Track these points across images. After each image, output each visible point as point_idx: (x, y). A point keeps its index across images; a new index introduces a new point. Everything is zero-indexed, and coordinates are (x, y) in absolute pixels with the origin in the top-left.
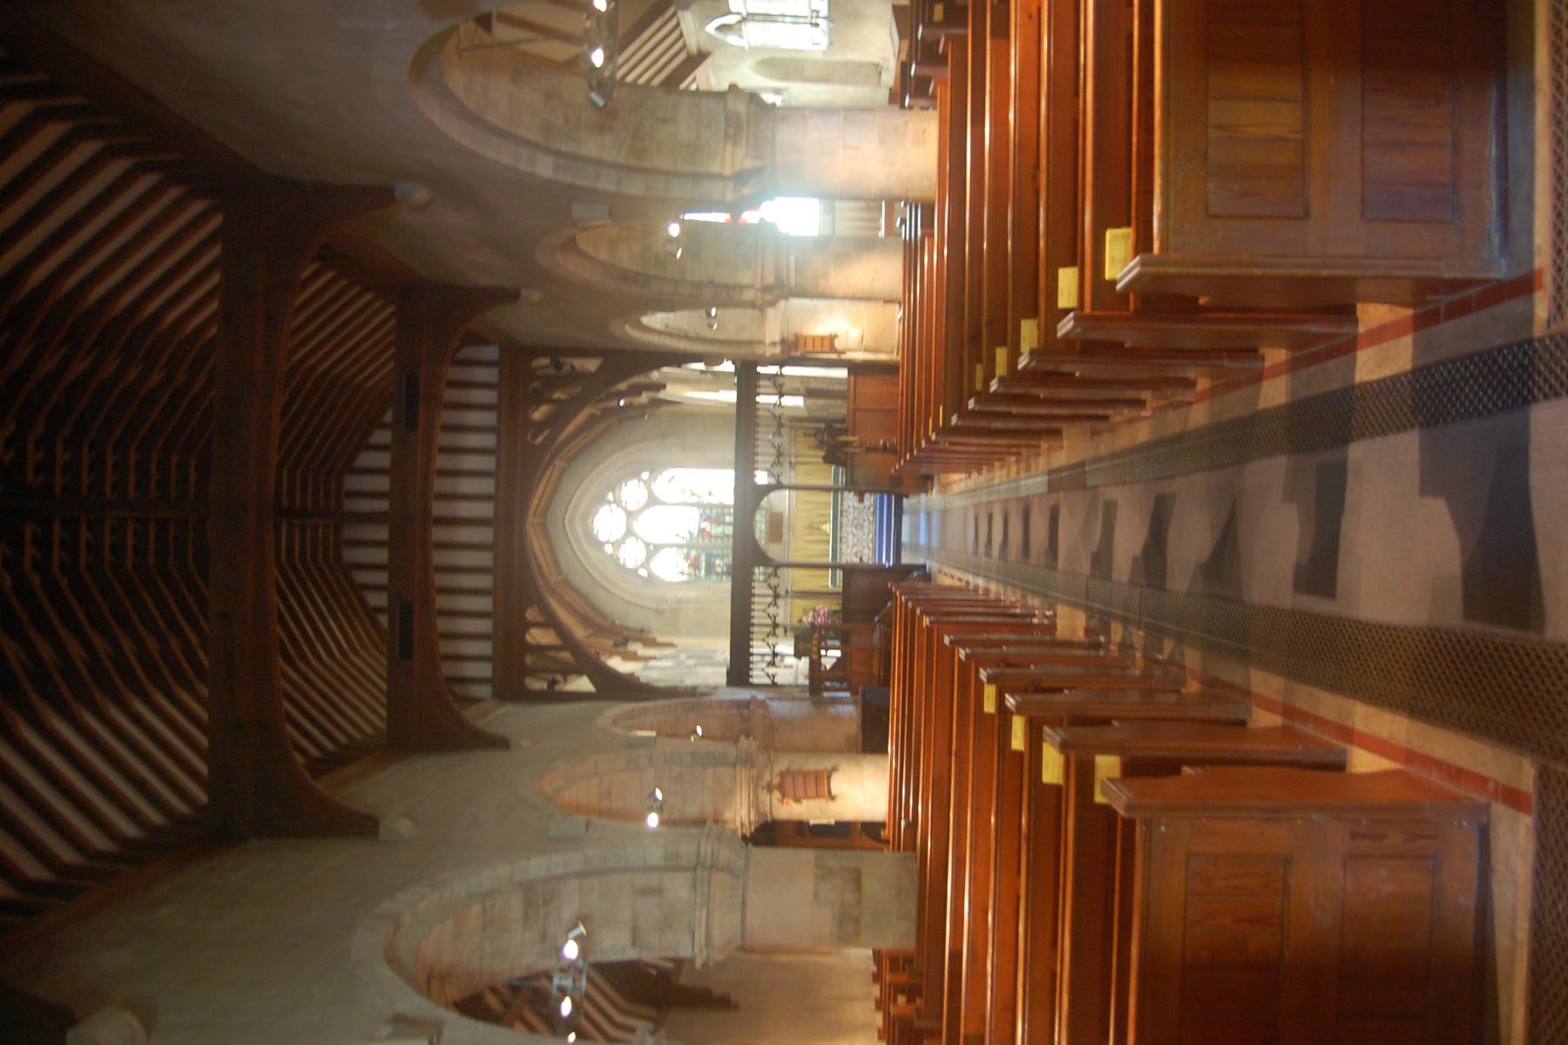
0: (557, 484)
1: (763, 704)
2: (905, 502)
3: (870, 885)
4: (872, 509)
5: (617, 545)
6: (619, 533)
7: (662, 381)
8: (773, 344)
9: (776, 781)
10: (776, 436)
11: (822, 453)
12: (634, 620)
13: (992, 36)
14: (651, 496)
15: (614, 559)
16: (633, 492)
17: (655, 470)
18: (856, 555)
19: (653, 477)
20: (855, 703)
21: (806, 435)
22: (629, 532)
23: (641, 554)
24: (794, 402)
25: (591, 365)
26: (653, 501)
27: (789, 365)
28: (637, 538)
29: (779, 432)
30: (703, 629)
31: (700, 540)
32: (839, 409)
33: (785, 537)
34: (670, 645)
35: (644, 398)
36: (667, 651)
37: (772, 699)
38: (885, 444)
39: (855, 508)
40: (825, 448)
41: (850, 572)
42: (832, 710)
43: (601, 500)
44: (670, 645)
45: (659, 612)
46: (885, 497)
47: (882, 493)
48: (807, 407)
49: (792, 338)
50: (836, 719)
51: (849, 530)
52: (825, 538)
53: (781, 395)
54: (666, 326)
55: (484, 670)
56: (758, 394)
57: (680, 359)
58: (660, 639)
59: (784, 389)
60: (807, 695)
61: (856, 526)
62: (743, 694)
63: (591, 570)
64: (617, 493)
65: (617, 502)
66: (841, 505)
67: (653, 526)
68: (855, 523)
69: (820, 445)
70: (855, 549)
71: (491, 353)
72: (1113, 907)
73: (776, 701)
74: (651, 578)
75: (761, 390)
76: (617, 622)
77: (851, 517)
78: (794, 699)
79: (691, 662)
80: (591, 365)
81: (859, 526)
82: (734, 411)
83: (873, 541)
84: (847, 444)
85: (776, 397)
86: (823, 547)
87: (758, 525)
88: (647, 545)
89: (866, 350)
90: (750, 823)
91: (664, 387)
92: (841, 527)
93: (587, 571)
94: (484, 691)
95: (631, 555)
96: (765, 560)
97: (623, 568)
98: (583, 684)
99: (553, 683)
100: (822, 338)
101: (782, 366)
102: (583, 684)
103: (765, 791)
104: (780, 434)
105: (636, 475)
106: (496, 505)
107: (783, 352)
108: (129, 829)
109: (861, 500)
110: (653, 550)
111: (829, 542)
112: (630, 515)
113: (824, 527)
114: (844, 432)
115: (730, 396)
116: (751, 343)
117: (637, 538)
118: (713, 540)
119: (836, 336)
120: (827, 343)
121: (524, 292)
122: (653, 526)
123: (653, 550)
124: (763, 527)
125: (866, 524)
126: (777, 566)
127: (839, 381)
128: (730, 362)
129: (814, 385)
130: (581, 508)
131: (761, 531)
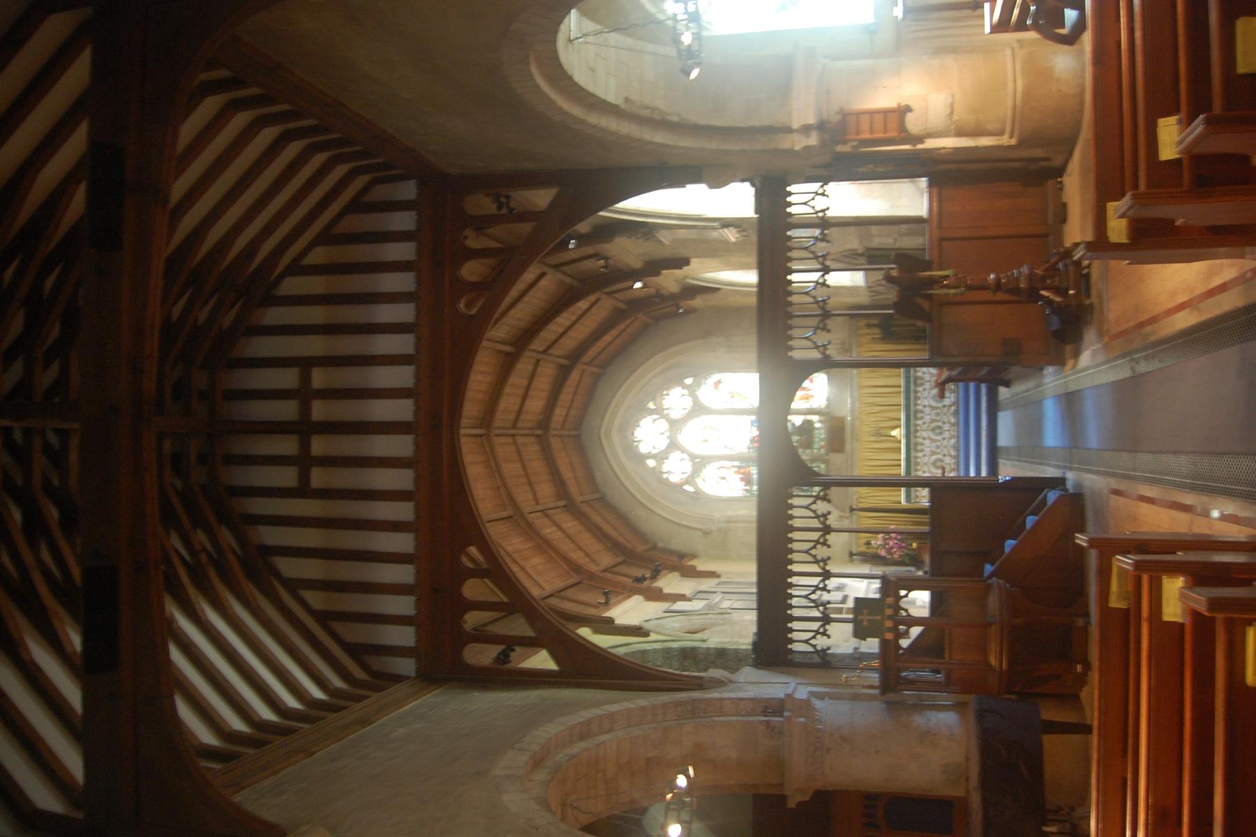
0: (591, 392)
1: (805, 707)
2: (1003, 392)
3: (922, 610)
4: (953, 408)
5: (661, 457)
6: (662, 444)
7: (684, 252)
8: (806, 129)
12: (677, 544)
15: (656, 473)
16: (676, 400)
17: (700, 373)
18: (934, 464)
19: (697, 384)
21: (869, 326)
22: (673, 445)
23: (688, 467)
25: (541, 198)
26: (698, 409)
28: (683, 451)
33: (848, 447)
34: (713, 574)
36: (707, 584)
37: (821, 697)
38: (998, 279)
39: (933, 408)
41: (939, 488)
42: (919, 720)
43: (643, 411)
44: (713, 574)
45: (706, 533)
46: (984, 388)
47: (979, 381)
49: (835, 118)
50: (927, 736)
51: (925, 434)
52: (896, 445)
54: (627, 100)
55: (404, 636)
58: (702, 566)
60: (877, 691)
61: (933, 430)
62: (775, 685)
63: (630, 488)
65: (659, 411)
67: (694, 436)
70: (934, 457)
71: (408, 190)
72: (749, 291)
74: (698, 496)
76: (660, 545)
77: (927, 419)
78: (855, 698)
80: (541, 198)
81: (938, 430)
83: (956, 448)
84: (933, 282)
86: (895, 456)
88: (693, 457)
89: (960, 133)
93: (626, 489)
94: (407, 666)
95: (676, 469)
97: (667, 483)
98: (542, 660)
99: (504, 657)
100: (886, 112)
102: (542, 660)
105: (678, 381)
106: (416, 403)
107: (823, 144)
108: (265, 713)
109: (942, 395)
110: (699, 462)
112: (675, 425)
113: (894, 433)
114: (928, 266)
116: (770, 130)
117: (683, 451)
119: (908, 109)
120: (893, 124)
122: (694, 436)
123: (699, 462)
125: (946, 427)
130: (617, 422)
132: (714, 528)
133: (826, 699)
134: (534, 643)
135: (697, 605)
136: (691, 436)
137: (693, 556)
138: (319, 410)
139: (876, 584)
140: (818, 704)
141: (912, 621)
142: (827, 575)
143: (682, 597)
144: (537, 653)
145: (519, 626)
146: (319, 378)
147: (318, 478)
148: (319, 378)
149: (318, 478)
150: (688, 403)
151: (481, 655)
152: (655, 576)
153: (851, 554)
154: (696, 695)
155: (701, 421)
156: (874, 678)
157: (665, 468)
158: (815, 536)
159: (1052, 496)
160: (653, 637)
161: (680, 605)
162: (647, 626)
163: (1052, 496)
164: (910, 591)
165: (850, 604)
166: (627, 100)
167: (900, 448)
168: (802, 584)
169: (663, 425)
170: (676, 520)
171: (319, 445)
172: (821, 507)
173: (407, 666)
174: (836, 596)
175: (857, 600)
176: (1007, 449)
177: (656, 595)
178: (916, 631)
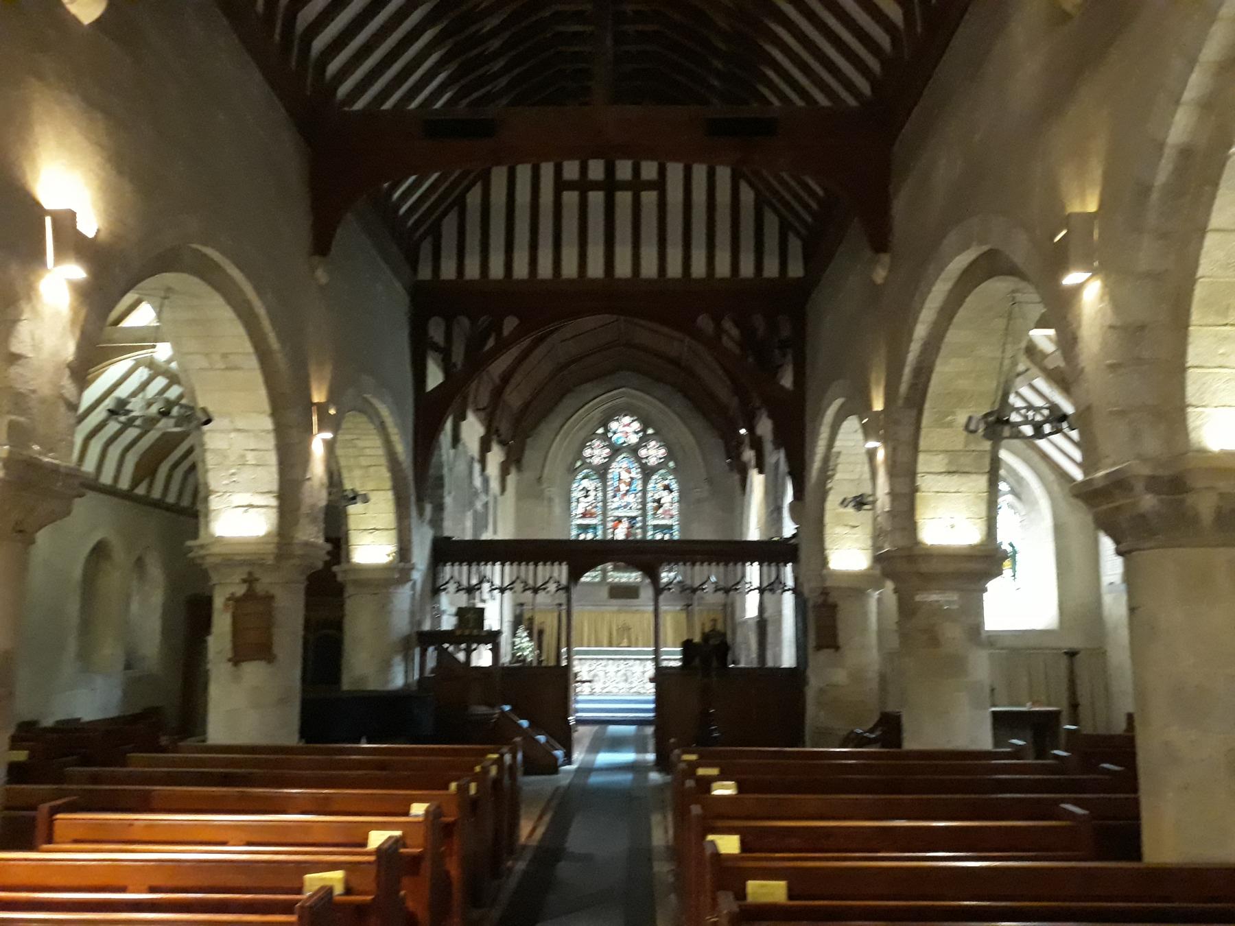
9: (260, 588)
10: (714, 586)
11: (697, 639)
12: (530, 456)
13: (804, 747)
14: (654, 470)
20: (406, 685)
21: (715, 620)
24: (751, 606)
26: (647, 472)
27: (796, 598)
29: (719, 590)
30: (521, 519)
31: (612, 518)
32: (746, 657)
33: (614, 601)
35: (749, 455)
36: (494, 485)
40: (984, 635)
48: (746, 622)
50: (386, 666)
52: (615, 642)
53: (761, 590)
55: (448, 271)
56: (761, 565)
57: (798, 473)
58: (512, 479)
59: (767, 595)
61: (625, 675)
64: (655, 437)
66: (635, 659)
68: (629, 674)
69: (706, 637)
71: (796, 270)
73: (412, 592)
75: (765, 568)
76: (529, 441)
79: (479, 506)
82: (737, 538)
85: (756, 584)
86: (605, 641)
87: (627, 575)
90: (203, 557)
91: (761, 472)
92: (625, 659)
94: (425, 273)
96: (575, 575)
98: (435, 378)
99: (436, 348)
101: (795, 591)
102: (435, 378)
103: (245, 576)
104: (717, 590)
110: (602, 472)
111: (611, 646)
112: (634, 450)
115: (753, 533)
118: (612, 530)
121: (885, 258)
124: (624, 580)
126: (567, 589)
127: (778, 656)
128: (795, 531)
129: (770, 629)
131: (621, 578)
132: (545, 486)
133: (412, 592)
134: (447, 368)
135: (478, 482)
136: (622, 468)
137: (519, 469)
138: (624, 199)
139: (495, 628)
140: (409, 585)
141: (469, 652)
142: (502, 590)
143: (483, 469)
144: (439, 366)
145: (458, 356)
146: (649, 198)
147: (571, 198)
148: (649, 198)
149: (571, 198)
150: (652, 462)
151: (436, 331)
152: (503, 443)
153: (522, 605)
154: (413, 499)
155: (636, 473)
156: (427, 627)
157: (596, 443)
158: (531, 582)
159: (559, 753)
160: (452, 452)
161: (477, 467)
162: (460, 447)
163: (559, 753)
164: (479, 644)
165: (480, 605)
166: (839, 453)
167: (582, 646)
168: (496, 572)
169: (634, 439)
170: (550, 455)
171: (596, 198)
172: (552, 587)
173: (425, 273)
174: (486, 596)
175: (482, 610)
176: (605, 729)
177: (485, 447)
178: (461, 656)
